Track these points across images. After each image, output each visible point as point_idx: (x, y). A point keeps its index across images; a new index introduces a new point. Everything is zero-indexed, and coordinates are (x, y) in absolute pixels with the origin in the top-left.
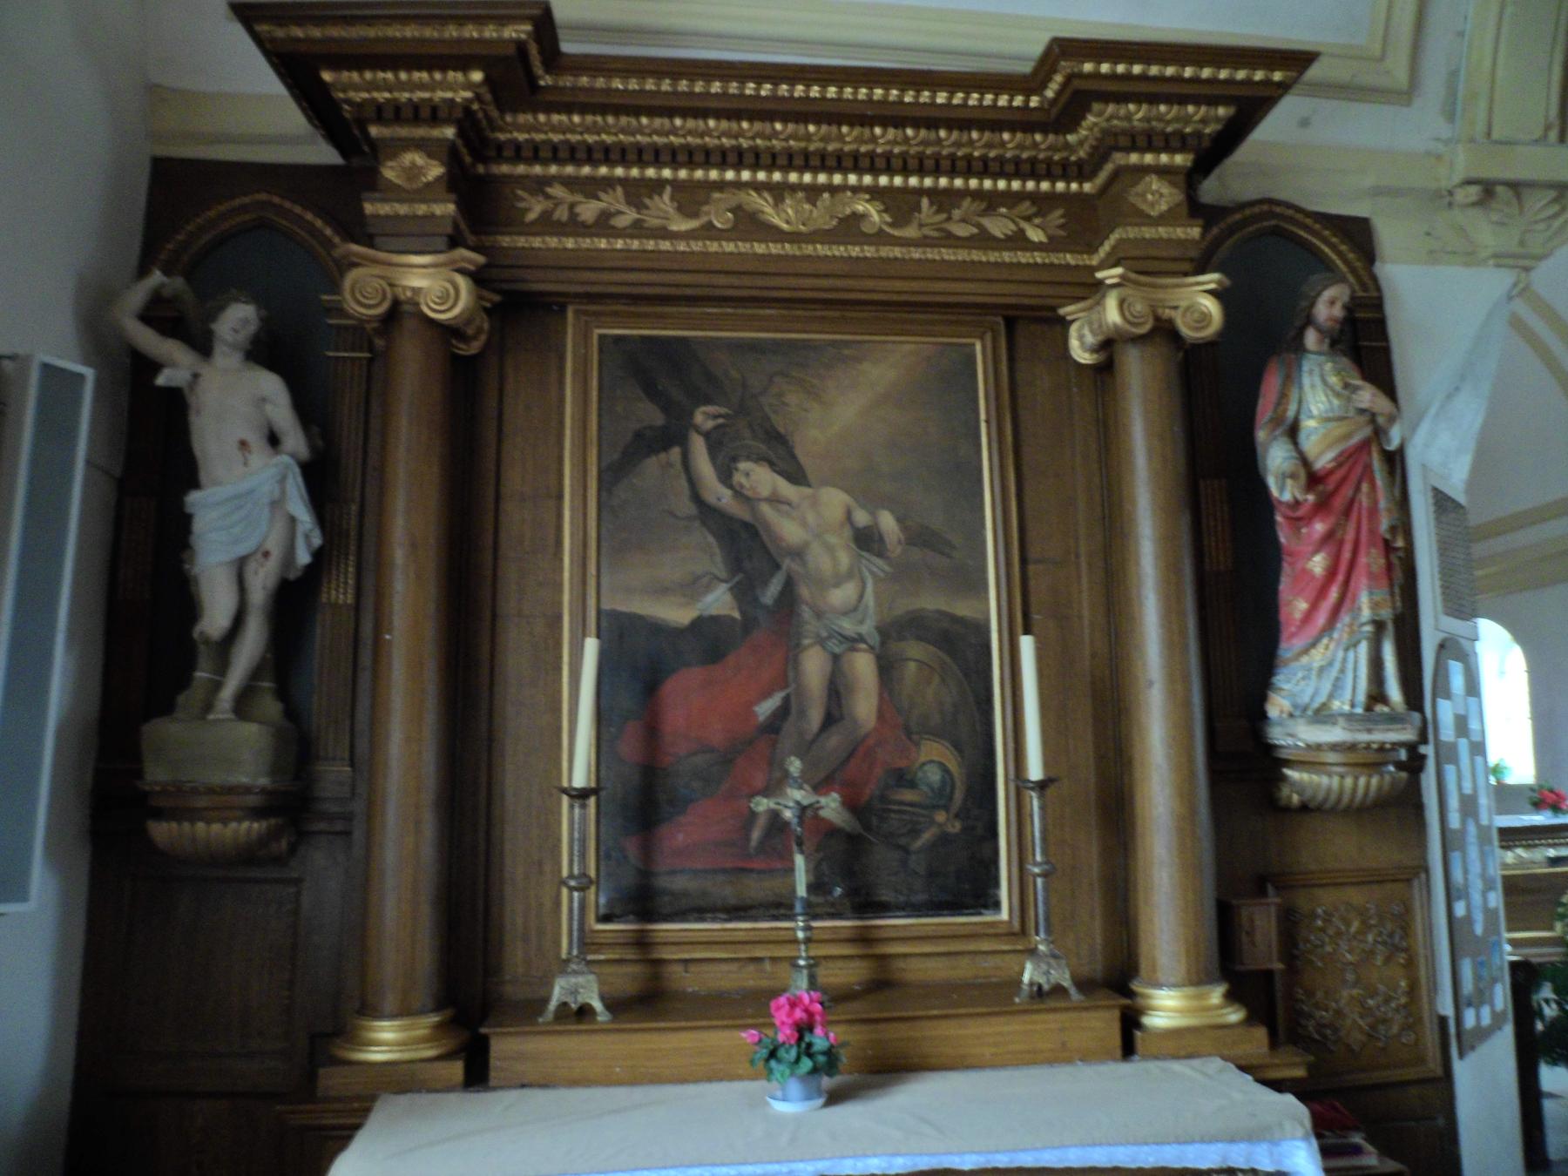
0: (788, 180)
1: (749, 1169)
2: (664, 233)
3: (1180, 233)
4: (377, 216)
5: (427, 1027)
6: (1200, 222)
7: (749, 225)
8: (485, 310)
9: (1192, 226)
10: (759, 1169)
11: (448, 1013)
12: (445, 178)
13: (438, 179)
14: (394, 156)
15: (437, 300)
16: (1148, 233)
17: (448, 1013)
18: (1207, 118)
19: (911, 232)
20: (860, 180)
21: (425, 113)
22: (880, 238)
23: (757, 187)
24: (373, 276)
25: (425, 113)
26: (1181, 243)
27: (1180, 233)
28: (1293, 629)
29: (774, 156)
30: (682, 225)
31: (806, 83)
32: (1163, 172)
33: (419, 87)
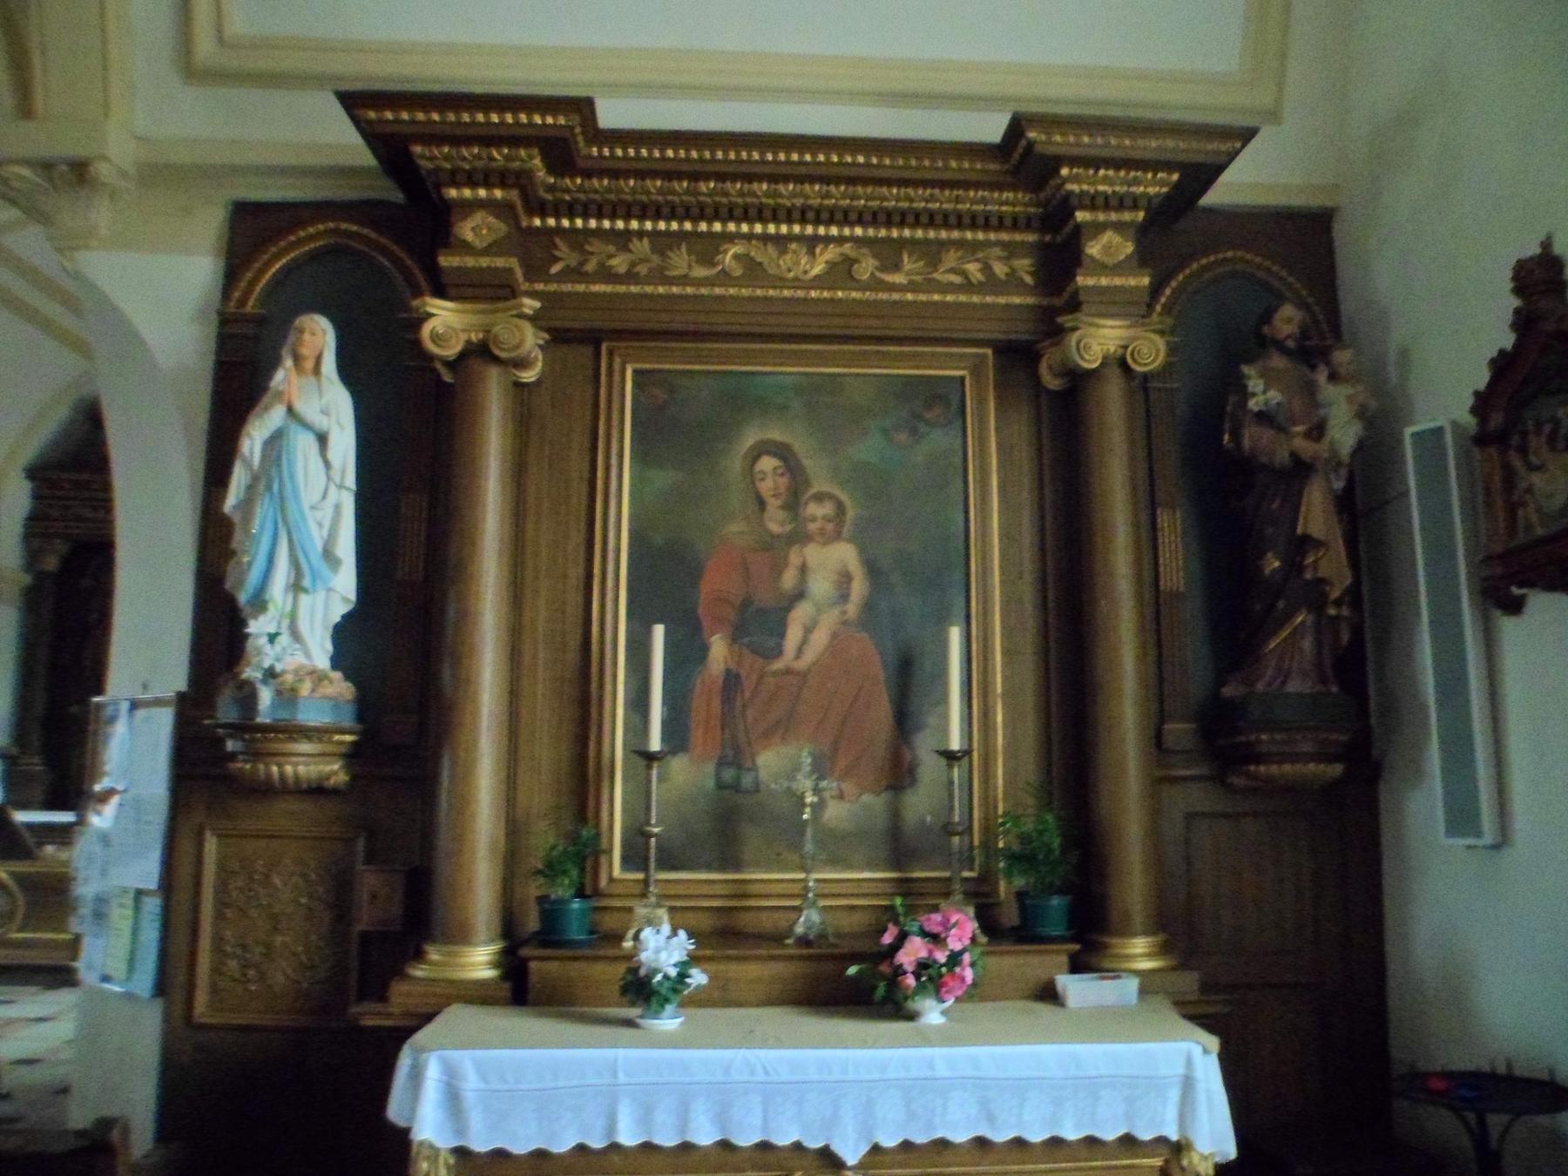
0: (639, 222)
1: (769, 1174)
2: (684, 280)
3: (1132, 282)
4: (1087, 288)
5: (1111, 956)
6: (1148, 270)
7: (753, 271)
8: (540, 346)
9: (1143, 276)
10: (773, 1174)
11: (1160, 938)
12: (1136, 257)
13: (1128, 258)
14: (1094, 236)
15: (1137, 349)
16: (470, 262)
17: (1160, 938)
18: (1154, 186)
19: (898, 279)
20: (751, 229)
21: (1100, 201)
22: (877, 285)
23: (765, 238)
24: (512, 316)
25: (1100, 201)
26: (1132, 290)
27: (1132, 282)
28: (1347, 599)
29: (673, 208)
30: (700, 272)
31: (879, 154)
32: (488, 205)
33: (1106, 182)
